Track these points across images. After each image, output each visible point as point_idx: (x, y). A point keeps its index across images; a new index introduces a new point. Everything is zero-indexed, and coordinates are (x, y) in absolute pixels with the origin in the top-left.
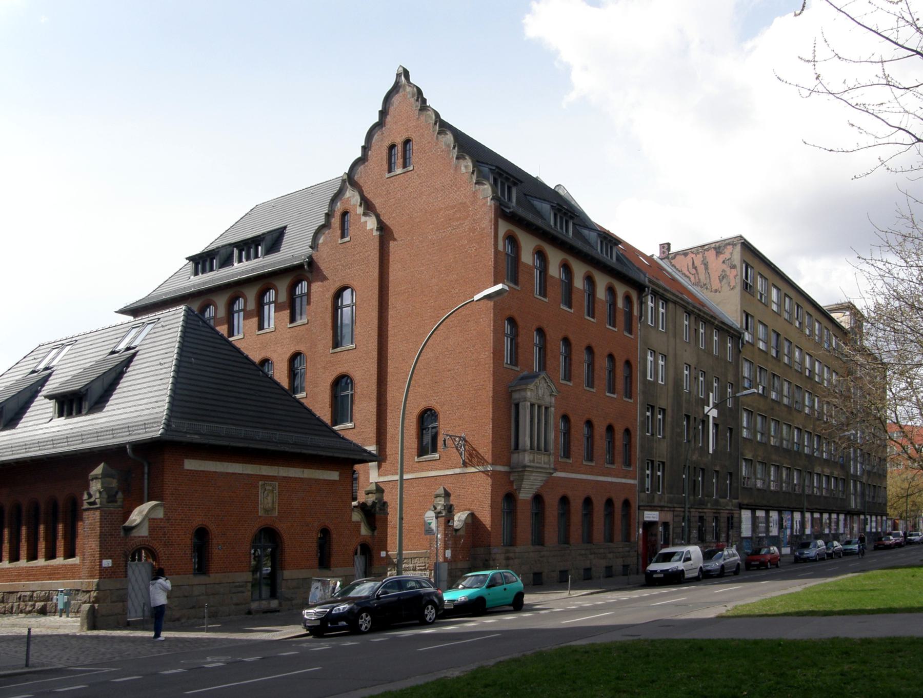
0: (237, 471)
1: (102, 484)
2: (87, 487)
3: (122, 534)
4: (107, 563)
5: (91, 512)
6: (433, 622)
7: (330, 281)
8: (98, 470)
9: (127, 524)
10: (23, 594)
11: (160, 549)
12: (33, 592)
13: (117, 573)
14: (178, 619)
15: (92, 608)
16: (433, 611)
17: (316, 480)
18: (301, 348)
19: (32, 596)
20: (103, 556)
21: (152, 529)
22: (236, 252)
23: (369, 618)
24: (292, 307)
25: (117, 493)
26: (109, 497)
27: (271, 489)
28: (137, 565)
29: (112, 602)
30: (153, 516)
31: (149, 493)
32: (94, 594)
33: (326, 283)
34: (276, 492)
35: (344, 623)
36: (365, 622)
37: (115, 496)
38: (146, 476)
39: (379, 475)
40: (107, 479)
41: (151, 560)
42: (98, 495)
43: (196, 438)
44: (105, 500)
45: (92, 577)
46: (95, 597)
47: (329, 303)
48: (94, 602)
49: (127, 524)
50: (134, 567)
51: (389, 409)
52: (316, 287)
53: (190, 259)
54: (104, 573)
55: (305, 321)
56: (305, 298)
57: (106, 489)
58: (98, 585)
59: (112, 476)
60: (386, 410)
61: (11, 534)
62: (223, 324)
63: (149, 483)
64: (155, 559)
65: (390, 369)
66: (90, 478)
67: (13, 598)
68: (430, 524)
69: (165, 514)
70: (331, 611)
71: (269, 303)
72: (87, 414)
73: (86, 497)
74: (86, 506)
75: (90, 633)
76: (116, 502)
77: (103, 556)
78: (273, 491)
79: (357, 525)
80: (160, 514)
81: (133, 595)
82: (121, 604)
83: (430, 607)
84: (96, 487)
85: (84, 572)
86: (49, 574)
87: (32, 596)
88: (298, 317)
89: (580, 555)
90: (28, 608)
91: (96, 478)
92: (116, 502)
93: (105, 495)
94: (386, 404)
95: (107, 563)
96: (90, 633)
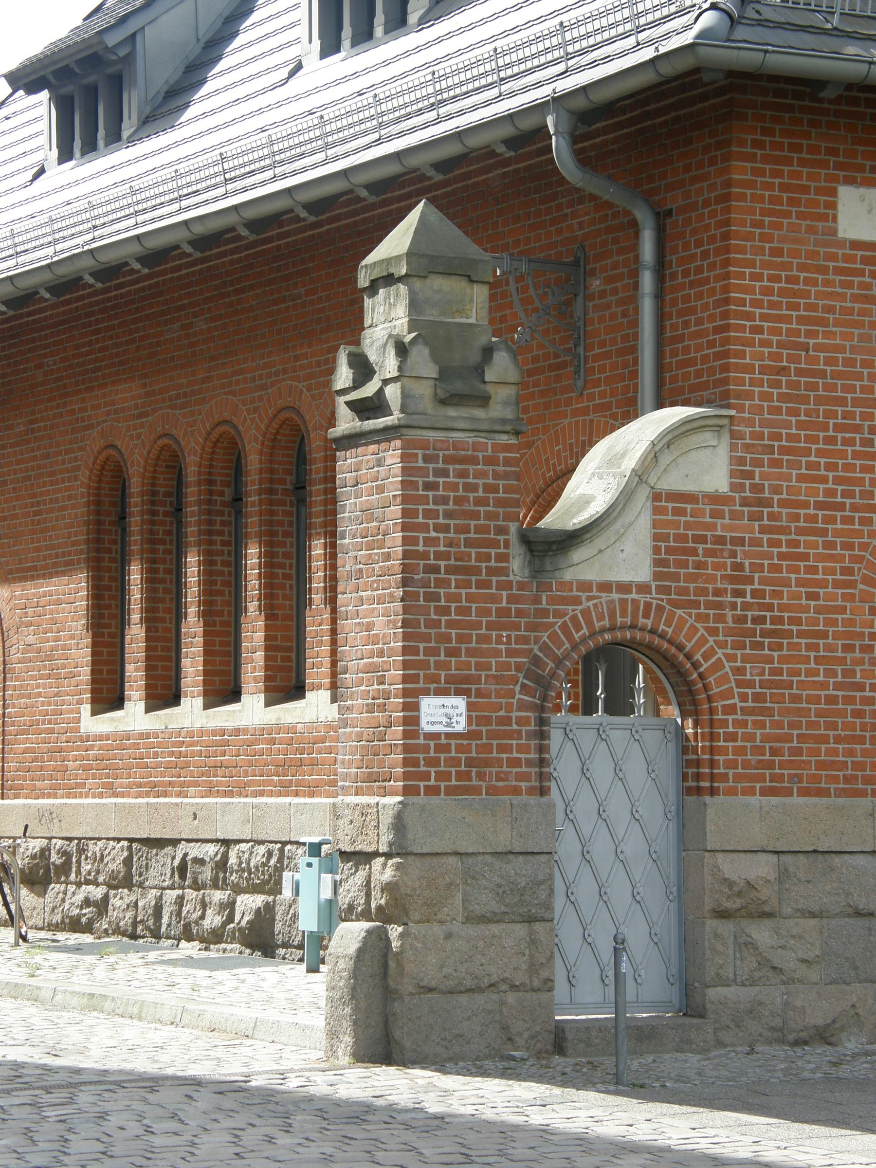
1: (414, 306)
2: (353, 325)
3: (517, 566)
4: (443, 713)
5: (366, 454)
8: (397, 242)
9: (552, 520)
10: (195, 851)
11: (716, 655)
12: (227, 843)
13: (491, 768)
14: (824, 1036)
15: (375, 948)
19: (222, 864)
20: (417, 683)
21: (669, 552)
25: (488, 352)
26: (444, 375)
30: (673, 482)
31: (660, 368)
32: (383, 872)
37: (479, 371)
38: (647, 280)
40: (438, 283)
41: (672, 711)
42: (390, 365)
44: (425, 390)
45: (373, 781)
46: (388, 888)
48: (385, 916)
49: (552, 520)
50: (587, 739)
54: (425, 766)
57: (429, 332)
58: (399, 824)
61: (151, 581)
63: (661, 318)
64: (690, 704)
66: (363, 282)
67: (160, 867)
69: (740, 473)
72: (425, 21)
73: (344, 376)
74: (346, 422)
76: (484, 400)
77: (417, 683)
80: (709, 470)
81: (586, 891)
82: (520, 930)
84: (386, 319)
85: (347, 759)
86: (283, 767)
87: (222, 864)
89: (617, 770)
90: (213, 920)
91: (389, 280)
92: (484, 400)
93: (424, 364)
95: (443, 713)
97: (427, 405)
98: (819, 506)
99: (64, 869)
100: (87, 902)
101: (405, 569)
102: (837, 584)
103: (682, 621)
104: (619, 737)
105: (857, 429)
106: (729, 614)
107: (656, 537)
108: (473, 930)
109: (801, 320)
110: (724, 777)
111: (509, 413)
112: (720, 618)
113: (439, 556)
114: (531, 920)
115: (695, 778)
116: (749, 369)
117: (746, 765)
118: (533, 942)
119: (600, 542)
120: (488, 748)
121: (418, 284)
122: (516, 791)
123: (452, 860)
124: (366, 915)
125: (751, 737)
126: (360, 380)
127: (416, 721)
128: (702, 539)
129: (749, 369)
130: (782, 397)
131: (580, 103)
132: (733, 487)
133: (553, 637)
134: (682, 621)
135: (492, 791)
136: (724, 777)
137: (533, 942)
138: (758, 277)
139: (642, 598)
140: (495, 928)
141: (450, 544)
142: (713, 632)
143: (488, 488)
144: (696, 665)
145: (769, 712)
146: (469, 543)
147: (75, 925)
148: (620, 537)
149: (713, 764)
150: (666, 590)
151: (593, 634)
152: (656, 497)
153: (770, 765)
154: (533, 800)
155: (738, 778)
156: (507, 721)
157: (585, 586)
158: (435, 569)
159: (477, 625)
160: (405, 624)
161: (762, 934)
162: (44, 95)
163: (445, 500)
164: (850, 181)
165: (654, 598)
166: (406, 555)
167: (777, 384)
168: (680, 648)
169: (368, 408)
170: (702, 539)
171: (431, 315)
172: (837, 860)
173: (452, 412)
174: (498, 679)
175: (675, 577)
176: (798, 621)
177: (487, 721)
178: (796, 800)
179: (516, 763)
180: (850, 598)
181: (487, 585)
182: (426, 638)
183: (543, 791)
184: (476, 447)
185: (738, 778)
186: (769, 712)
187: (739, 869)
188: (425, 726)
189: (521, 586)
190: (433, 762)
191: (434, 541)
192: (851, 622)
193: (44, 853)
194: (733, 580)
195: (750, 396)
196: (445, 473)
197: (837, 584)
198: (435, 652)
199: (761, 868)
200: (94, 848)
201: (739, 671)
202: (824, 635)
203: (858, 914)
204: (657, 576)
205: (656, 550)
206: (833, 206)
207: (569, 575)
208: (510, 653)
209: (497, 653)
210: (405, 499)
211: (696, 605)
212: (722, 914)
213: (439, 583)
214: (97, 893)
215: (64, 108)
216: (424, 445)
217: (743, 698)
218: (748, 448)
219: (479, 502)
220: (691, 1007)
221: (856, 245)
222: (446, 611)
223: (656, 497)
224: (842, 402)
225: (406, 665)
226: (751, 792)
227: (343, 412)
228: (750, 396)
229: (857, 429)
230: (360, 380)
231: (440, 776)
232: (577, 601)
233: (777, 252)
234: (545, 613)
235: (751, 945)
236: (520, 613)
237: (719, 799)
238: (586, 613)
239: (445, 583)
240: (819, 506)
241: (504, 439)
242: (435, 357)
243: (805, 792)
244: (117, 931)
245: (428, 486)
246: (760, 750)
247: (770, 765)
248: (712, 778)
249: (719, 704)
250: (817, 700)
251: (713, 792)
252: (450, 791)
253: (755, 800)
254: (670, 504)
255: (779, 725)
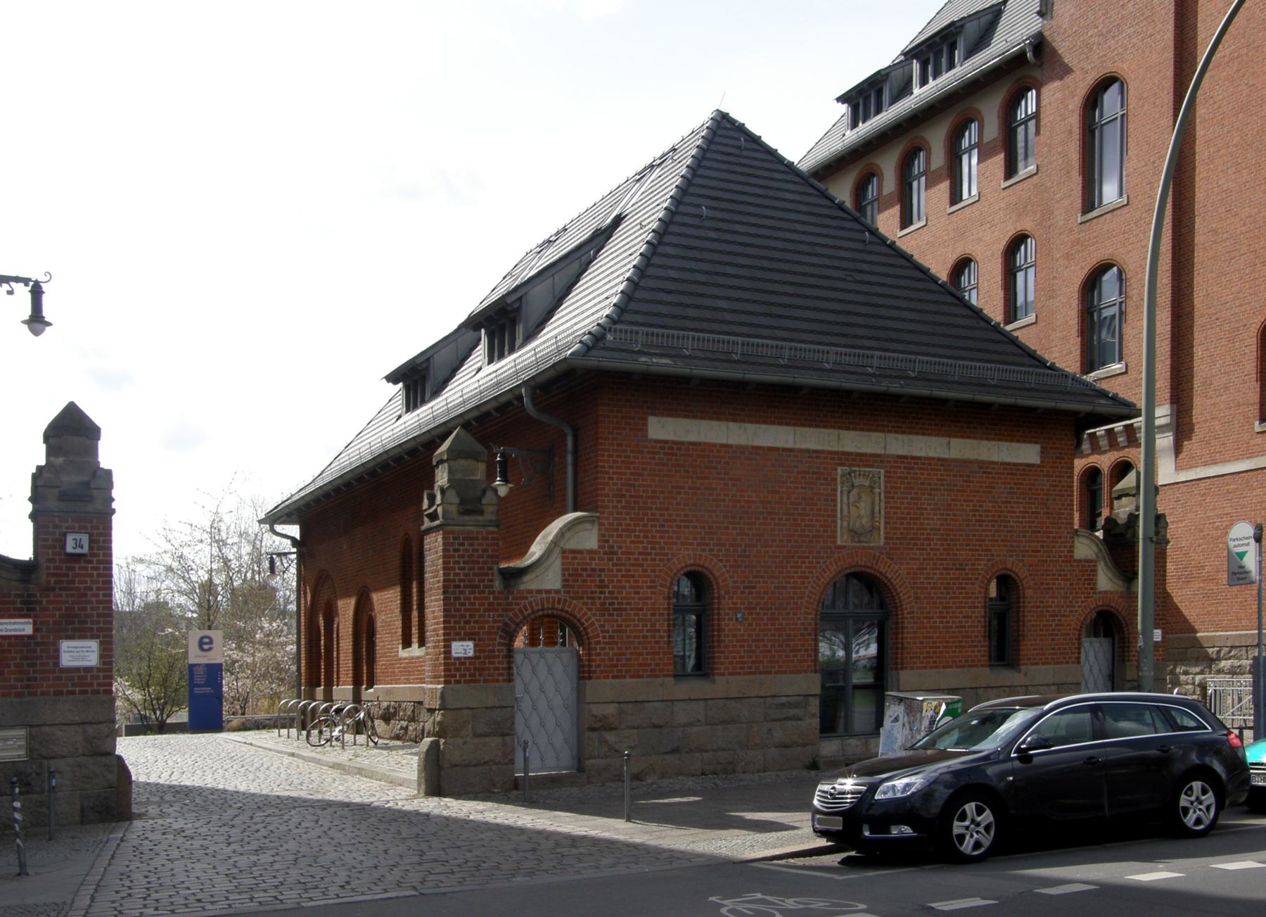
0: (779, 444)
1: (450, 472)
3: (498, 584)
4: (464, 649)
6: (1213, 825)
7: (1078, 74)
11: (591, 619)
16: (1209, 798)
17: (982, 465)
18: (1027, 225)
22: (916, 66)
23: (987, 817)
24: (1009, 149)
26: (462, 502)
27: (864, 483)
28: (541, 654)
29: (476, 735)
30: (572, 545)
32: (438, 717)
33: (1068, 80)
34: (880, 490)
35: (907, 830)
36: (974, 827)
37: (480, 499)
38: (570, 458)
39: (1178, 468)
40: (462, 462)
41: (576, 644)
43: (662, 364)
44: (454, 509)
47: (1074, 121)
50: (535, 658)
51: (1199, 322)
52: (1052, 91)
53: (842, 99)
54: (453, 671)
55: (1032, 168)
56: (1032, 124)
58: (443, 697)
59: (473, 456)
60: (1192, 327)
62: (892, 206)
65: (1201, 237)
68: (1241, 555)
69: (603, 540)
70: (873, 788)
71: (969, 150)
73: (426, 503)
75: (433, 806)
76: (481, 513)
77: (451, 634)
78: (872, 488)
79: (1088, 569)
80: (589, 540)
82: (499, 739)
83: (1197, 785)
84: (442, 478)
88: (1021, 165)
89: (534, 672)
92: (481, 513)
93: (453, 498)
94: (1191, 314)
95: (464, 649)
96: (433, 806)
97: (455, 515)
98: (640, 554)
99: (395, 714)
100: (402, 728)
101: (444, 587)
102: (648, 587)
103: (576, 606)
104: (549, 656)
105: (657, 520)
106: (598, 602)
107: (564, 570)
108: (476, 740)
109: (631, 474)
110: (595, 672)
111: (493, 518)
112: (594, 604)
113: (460, 580)
114: (503, 735)
115: (584, 672)
116: (608, 495)
117: (605, 666)
118: (505, 744)
119: (537, 572)
120: (484, 663)
121: (452, 463)
122: (497, 681)
123: (467, 712)
124: (434, 735)
125: (607, 654)
126: (430, 506)
127: (450, 652)
128: (586, 570)
129: (608, 495)
130: (623, 507)
131: (532, 383)
132: (600, 547)
133: (515, 614)
134: (576, 606)
135: (486, 681)
136: (595, 672)
137: (505, 744)
138: (610, 456)
139: (557, 596)
140: (487, 739)
141: (466, 575)
142: (590, 610)
143: (484, 551)
144: (582, 624)
145: (616, 643)
146: (475, 575)
147: (397, 737)
148: (546, 570)
149: (590, 666)
150: (568, 592)
151: (534, 612)
152: (564, 552)
153: (616, 666)
154: (505, 684)
155: (601, 672)
156: (493, 651)
157: (530, 592)
158: (459, 586)
159: (478, 610)
160: (445, 610)
161: (611, 737)
162: (400, 385)
163: (463, 556)
164: (654, 414)
165: (562, 596)
166: (445, 581)
167: (620, 502)
168: (575, 617)
169: (433, 517)
170: (586, 570)
171: (458, 476)
172: (646, 705)
173: (466, 518)
174: (489, 633)
175: (573, 587)
176: (629, 604)
177: (483, 651)
178: (628, 680)
179: (497, 669)
180: (654, 593)
181: (483, 592)
182: (454, 616)
183: (510, 680)
184: (478, 533)
185: (601, 672)
186: (616, 643)
187: (599, 711)
188: (454, 654)
189: (499, 593)
190: (459, 670)
191: (458, 574)
192: (654, 604)
193: (388, 707)
194: (599, 587)
195: (608, 507)
196: (463, 544)
197: (648, 587)
198: (459, 622)
199: (610, 710)
200: (404, 705)
201: (603, 626)
202: (642, 609)
203: (655, 726)
204: (564, 586)
205: (564, 575)
206: (646, 425)
207: (522, 587)
208: (494, 622)
209: (488, 622)
210: (444, 556)
211: (582, 598)
212: (593, 729)
213: (461, 592)
214: (404, 723)
215: (407, 388)
216: (453, 532)
217: (604, 637)
218: (606, 530)
219: (479, 556)
220: (580, 769)
221: (657, 441)
222: (464, 604)
223: (564, 552)
224: (651, 509)
225: (445, 628)
226: (607, 677)
227: (426, 519)
228: (608, 507)
229: (657, 520)
230: (430, 506)
231: (461, 676)
232: (526, 598)
233: (620, 445)
234: (511, 604)
235: (606, 742)
236: (499, 604)
237: (593, 681)
238: (530, 603)
239: (463, 592)
240: (640, 554)
241: (491, 529)
242: (458, 494)
243: (631, 677)
244: (411, 740)
245: (455, 550)
246: (611, 660)
247: (616, 666)
248: (589, 672)
249: (593, 641)
250: (638, 637)
251: (590, 678)
252: (466, 682)
253: (608, 681)
254: (570, 556)
255: (620, 649)
